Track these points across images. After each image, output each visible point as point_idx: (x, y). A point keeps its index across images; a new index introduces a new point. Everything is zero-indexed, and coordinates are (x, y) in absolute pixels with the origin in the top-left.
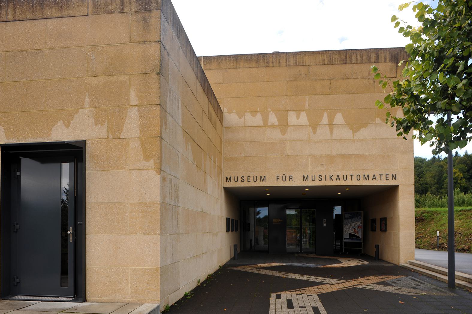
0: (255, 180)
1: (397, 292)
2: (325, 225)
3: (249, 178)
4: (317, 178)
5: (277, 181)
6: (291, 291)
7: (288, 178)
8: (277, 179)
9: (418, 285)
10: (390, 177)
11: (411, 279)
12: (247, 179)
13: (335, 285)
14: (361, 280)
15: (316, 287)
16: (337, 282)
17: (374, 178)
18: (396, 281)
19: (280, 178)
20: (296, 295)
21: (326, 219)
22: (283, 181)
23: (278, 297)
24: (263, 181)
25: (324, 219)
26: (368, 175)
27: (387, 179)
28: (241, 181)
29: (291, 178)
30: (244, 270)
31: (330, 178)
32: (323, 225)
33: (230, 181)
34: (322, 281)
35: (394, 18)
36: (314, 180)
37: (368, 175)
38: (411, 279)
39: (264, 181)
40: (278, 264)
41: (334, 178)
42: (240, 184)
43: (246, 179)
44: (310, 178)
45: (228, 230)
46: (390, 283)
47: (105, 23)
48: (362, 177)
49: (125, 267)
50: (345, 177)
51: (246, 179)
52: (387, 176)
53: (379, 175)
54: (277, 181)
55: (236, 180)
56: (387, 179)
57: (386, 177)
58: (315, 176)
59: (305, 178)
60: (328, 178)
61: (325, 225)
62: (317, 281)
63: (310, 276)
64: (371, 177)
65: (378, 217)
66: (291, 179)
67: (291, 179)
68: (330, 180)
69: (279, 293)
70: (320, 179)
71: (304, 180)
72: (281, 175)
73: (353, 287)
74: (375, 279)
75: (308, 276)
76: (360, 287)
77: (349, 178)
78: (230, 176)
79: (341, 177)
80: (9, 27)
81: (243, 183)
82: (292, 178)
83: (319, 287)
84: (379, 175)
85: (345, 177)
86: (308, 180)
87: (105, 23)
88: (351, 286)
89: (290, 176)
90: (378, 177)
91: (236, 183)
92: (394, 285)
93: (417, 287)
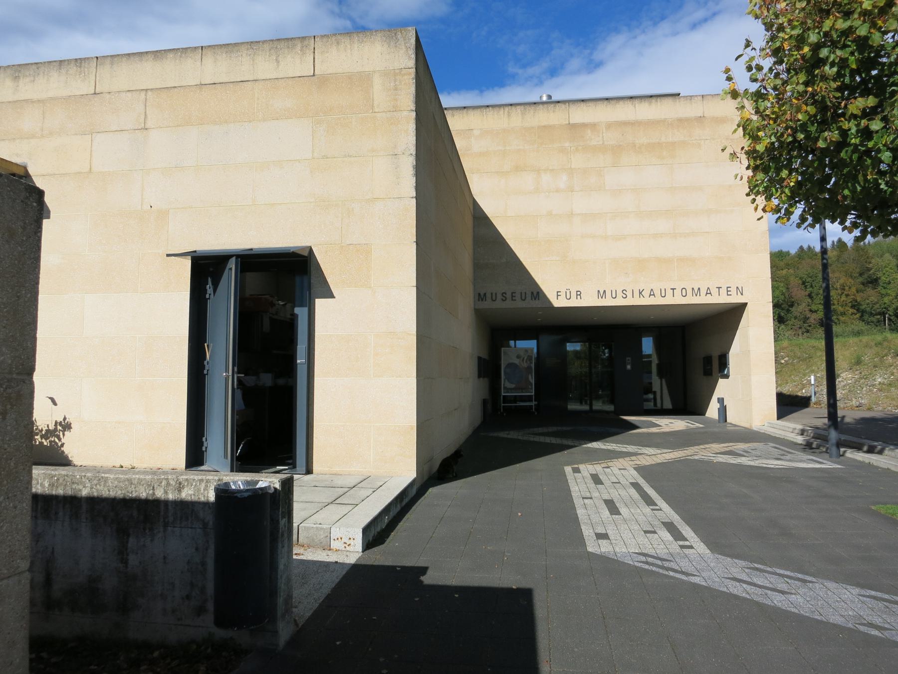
0: (523, 298)
1: (752, 463)
2: (629, 367)
3: (559, 294)
4: (620, 294)
5: (557, 299)
6: (593, 463)
7: (574, 295)
8: (558, 295)
9: (783, 455)
10: (733, 291)
11: (772, 447)
12: (511, 297)
13: (657, 456)
14: (695, 449)
15: (628, 459)
16: (659, 452)
17: (708, 293)
18: (750, 451)
19: (563, 294)
20: (601, 468)
21: (630, 358)
22: (567, 299)
23: (576, 470)
24: (535, 299)
25: (627, 358)
26: (699, 289)
27: (729, 293)
28: (622, 296)
29: (579, 294)
30: (509, 437)
31: (640, 293)
32: (625, 367)
33: (484, 300)
34: (636, 450)
35: (727, 70)
36: (685, 295)
37: (699, 289)
38: (772, 447)
39: (537, 299)
40: (559, 428)
41: (646, 293)
42: (499, 305)
43: (509, 296)
44: (608, 294)
45: (479, 376)
46: (741, 453)
47: (338, 86)
48: (689, 292)
49: (365, 424)
50: (494, 295)
51: (509, 296)
52: (514, 295)
53: (717, 288)
54: (557, 299)
55: (494, 298)
56: (729, 293)
57: (728, 291)
58: (616, 291)
59: (602, 294)
60: (636, 294)
61: (629, 367)
62: (627, 451)
63: (615, 445)
64: (703, 292)
65: (715, 354)
66: (579, 297)
67: (579, 297)
68: (640, 297)
69: (576, 466)
70: (624, 296)
71: (533, 299)
72: (563, 291)
73: (684, 458)
74: (716, 447)
75: (612, 444)
76: (696, 457)
77: (669, 292)
78: (485, 292)
79: (657, 293)
80: (205, 92)
81: (504, 302)
82: (580, 295)
83: (633, 458)
84: (717, 288)
85: (494, 295)
86: (605, 298)
87: (338, 86)
88: (683, 457)
89: (577, 292)
90: (714, 291)
91: (494, 302)
92: (747, 455)
93: (782, 457)
